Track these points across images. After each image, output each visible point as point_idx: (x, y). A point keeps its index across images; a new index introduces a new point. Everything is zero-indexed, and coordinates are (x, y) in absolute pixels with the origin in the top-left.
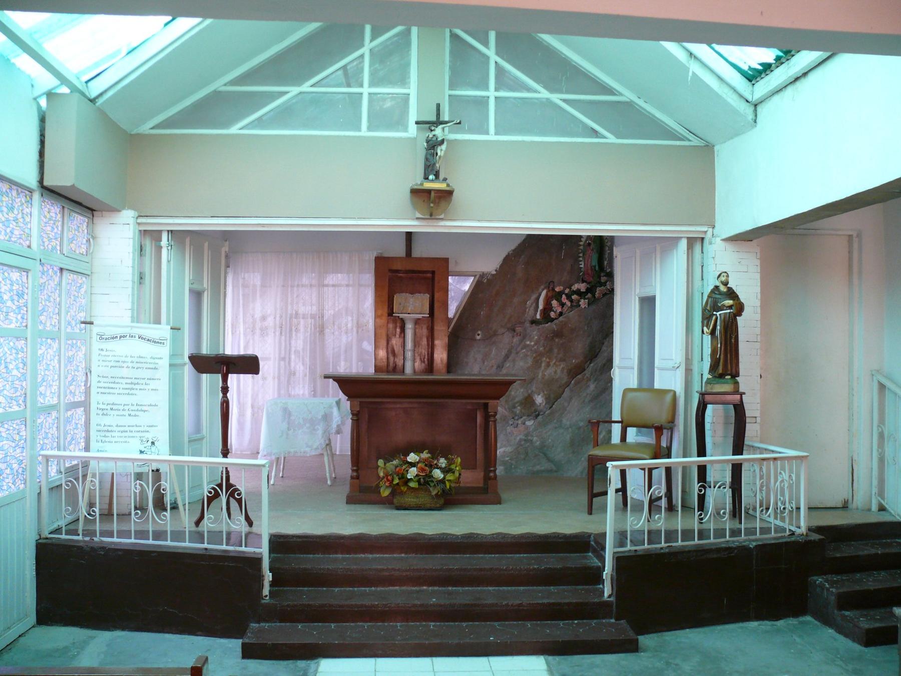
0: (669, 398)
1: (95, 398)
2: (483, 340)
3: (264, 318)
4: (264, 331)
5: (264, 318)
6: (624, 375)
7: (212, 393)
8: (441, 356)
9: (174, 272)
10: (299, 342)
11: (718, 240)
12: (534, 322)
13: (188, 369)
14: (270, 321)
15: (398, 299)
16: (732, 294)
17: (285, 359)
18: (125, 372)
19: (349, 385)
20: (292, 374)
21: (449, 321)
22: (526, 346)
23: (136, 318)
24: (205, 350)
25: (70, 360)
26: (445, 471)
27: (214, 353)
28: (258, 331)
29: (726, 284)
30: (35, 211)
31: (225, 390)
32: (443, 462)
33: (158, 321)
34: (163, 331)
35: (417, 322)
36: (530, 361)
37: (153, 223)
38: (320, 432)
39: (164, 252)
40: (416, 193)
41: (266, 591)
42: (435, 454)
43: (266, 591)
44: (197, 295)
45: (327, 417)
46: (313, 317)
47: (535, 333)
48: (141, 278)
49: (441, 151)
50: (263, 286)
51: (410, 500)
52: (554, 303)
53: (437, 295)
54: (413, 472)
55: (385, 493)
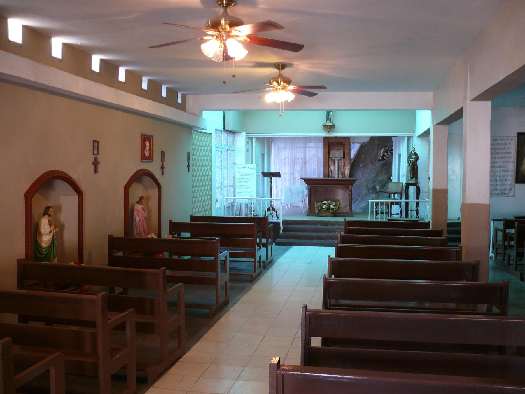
0: (401, 185)
1: (237, 184)
2: (363, 167)
3: (285, 159)
4: (285, 164)
5: (285, 159)
6: (394, 179)
7: (267, 185)
8: (347, 172)
9: (257, 148)
10: (298, 167)
11: (415, 137)
12: (379, 161)
13: (261, 176)
14: (287, 160)
15: (332, 152)
16: (416, 154)
17: (292, 174)
18: (244, 177)
19: (308, 181)
20: (294, 179)
21: (350, 159)
22: (374, 169)
23: (247, 162)
24: (265, 171)
25: (230, 174)
26: (334, 206)
27: (268, 172)
28: (282, 164)
29: (414, 151)
30: (223, 136)
31: (271, 182)
32: (334, 203)
33: (252, 163)
34: (254, 166)
35: (339, 160)
36: (375, 174)
37: (250, 135)
38: (301, 196)
39: (254, 143)
40: (325, 126)
41: (281, 231)
42: (332, 201)
43: (281, 231)
44: (263, 155)
45: (303, 192)
46: (302, 159)
47: (378, 164)
48: (247, 151)
49: (331, 114)
50: (284, 148)
51: (324, 214)
52: (385, 154)
53: (346, 151)
54: (325, 206)
55: (317, 212)
